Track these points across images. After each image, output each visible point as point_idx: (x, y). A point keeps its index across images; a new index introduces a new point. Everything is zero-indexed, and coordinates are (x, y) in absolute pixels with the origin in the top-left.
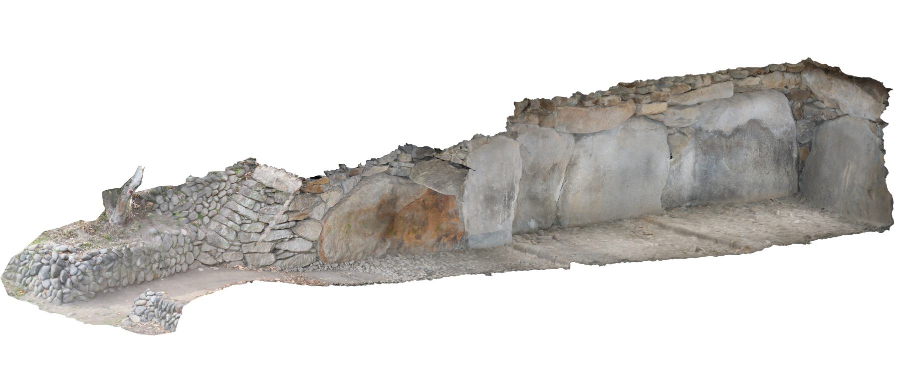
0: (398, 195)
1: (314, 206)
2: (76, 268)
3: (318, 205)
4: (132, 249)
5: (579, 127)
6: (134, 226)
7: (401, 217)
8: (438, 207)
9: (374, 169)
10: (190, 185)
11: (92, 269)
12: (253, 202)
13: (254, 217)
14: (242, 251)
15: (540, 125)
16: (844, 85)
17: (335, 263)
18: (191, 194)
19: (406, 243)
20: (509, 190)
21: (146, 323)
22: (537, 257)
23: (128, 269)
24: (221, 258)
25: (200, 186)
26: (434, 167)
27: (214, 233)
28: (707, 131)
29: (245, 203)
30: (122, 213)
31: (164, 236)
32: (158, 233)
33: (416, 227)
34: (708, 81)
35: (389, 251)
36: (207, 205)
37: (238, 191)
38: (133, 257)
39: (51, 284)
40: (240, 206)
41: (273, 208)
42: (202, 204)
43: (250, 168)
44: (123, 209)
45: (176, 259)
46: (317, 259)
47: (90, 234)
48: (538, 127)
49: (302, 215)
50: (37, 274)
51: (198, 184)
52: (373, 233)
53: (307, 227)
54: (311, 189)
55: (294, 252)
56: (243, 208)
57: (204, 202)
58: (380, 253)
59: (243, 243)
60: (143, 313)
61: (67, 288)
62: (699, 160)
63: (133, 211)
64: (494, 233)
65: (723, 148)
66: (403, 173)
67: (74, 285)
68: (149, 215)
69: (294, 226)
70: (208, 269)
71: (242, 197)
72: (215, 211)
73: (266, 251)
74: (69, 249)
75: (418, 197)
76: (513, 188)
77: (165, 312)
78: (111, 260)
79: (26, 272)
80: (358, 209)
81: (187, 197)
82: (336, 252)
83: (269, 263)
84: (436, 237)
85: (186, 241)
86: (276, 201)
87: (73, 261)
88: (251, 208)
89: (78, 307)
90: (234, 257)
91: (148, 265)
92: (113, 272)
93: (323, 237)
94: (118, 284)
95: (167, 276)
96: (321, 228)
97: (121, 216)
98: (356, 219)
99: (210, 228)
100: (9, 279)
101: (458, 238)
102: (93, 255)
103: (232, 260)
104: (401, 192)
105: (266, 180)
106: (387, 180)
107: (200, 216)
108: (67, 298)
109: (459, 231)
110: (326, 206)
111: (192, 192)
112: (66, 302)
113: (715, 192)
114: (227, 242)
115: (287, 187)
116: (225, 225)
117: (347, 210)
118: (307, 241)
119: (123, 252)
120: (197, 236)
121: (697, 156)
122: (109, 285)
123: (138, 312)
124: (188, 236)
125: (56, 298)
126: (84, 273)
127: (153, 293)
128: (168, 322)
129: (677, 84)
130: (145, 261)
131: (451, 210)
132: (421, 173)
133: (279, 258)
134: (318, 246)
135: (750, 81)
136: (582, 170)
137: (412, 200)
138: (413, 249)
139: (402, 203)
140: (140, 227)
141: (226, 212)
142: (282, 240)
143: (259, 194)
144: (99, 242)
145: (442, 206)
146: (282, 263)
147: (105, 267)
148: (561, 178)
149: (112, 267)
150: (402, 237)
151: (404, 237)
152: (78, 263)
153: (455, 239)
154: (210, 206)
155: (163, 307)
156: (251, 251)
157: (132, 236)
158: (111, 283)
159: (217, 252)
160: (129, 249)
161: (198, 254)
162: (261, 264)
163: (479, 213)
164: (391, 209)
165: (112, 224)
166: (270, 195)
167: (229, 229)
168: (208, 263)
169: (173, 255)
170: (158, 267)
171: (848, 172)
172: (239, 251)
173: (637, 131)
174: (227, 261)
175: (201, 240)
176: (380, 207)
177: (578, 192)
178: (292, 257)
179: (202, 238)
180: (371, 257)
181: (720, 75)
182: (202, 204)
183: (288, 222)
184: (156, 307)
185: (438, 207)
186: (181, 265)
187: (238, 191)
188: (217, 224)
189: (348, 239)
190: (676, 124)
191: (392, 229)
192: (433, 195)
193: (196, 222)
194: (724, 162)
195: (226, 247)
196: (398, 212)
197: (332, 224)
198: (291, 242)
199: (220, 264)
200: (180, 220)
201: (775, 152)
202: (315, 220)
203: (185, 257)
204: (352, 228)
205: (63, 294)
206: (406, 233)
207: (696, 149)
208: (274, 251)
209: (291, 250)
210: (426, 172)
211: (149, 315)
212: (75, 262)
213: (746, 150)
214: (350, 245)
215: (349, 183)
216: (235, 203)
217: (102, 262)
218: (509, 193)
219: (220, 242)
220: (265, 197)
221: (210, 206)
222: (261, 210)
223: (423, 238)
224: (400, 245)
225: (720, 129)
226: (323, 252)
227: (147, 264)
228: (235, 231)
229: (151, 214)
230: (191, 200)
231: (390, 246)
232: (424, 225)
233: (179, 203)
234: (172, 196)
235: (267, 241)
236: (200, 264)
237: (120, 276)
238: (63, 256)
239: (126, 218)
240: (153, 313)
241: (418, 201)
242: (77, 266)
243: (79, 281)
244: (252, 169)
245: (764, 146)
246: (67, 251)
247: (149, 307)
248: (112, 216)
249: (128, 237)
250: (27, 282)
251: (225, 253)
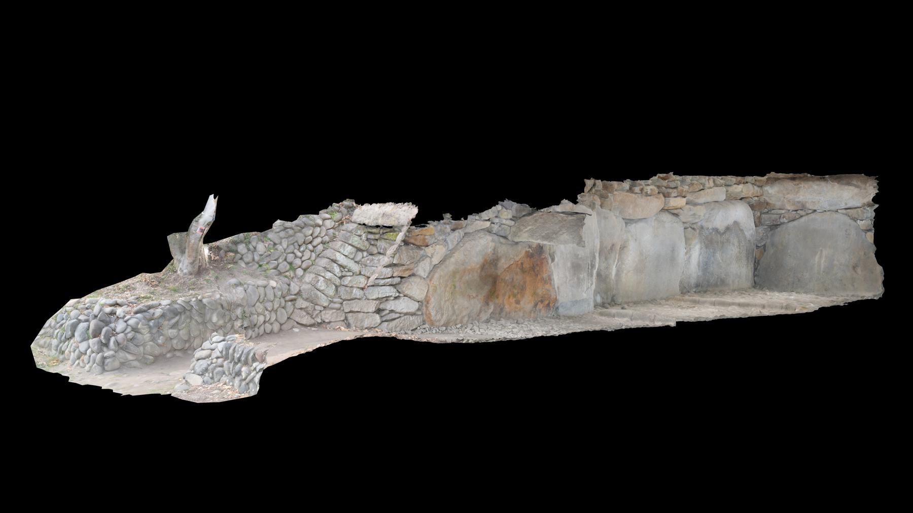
0: (499, 255)
1: (419, 261)
2: (125, 324)
3: (423, 260)
4: (205, 301)
5: (630, 212)
6: (211, 276)
7: (502, 280)
8: (534, 271)
10: (278, 230)
11: (148, 325)
12: (354, 250)
13: (355, 268)
14: (343, 310)
16: (817, 185)
17: (442, 326)
18: (279, 241)
19: (507, 308)
20: (592, 259)
21: (211, 386)
22: (629, 320)
23: (201, 327)
24: (320, 317)
25: (291, 232)
26: (540, 220)
27: (310, 286)
29: (344, 250)
30: (193, 259)
31: (248, 287)
32: (240, 284)
33: (516, 291)
35: (493, 314)
36: (299, 254)
37: (335, 237)
38: (207, 311)
39: (89, 347)
40: (339, 254)
41: (376, 258)
42: (293, 253)
43: (348, 211)
44: (194, 254)
45: (265, 316)
46: (424, 323)
47: (153, 286)
49: (407, 270)
50: (73, 335)
51: (287, 228)
52: (477, 296)
53: (413, 284)
54: (416, 240)
55: (400, 313)
56: (343, 256)
57: (296, 251)
58: (484, 317)
59: (344, 300)
60: (206, 370)
61: (111, 350)
63: (210, 263)
65: (718, 242)
66: (503, 232)
67: (121, 346)
68: (229, 267)
69: (399, 284)
70: (305, 329)
71: (340, 243)
72: (310, 262)
73: (370, 311)
74: (119, 301)
75: (517, 259)
76: (594, 257)
77: (239, 365)
78: (176, 313)
79: (62, 336)
81: (275, 244)
82: (442, 315)
83: (374, 325)
84: (533, 302)
85: (276, 294)
86: (379, 250)
87: (122, 316)
88: (352, 257)
89: (125, 375)
90: (335, 317)
91: (228, 322)
92: (179, 330)
93: (429, 297)
94: (187, 345)
95: (254, 336)
96: (427, 287)
97: (192, 263)
98: (461, 278)
99: (305, 281)
100: (43, 347)
101: (551, 305)
102: (150, 307)
103: (332, 320)
105: (370, 218)
106: (489, 238)
107: (292, 266)
108: (109, 364)
109: (552, 297)
110: (431, 262)
111: (281, 238)
112: (109, 369)
113: (712, 281)
114: (325, 297)
115: (398, 219)
116: (323, 277)
117: (452, 268)
118: (413, 301)
119: (192, 303)
120: (289, 290)
121: (701, 249)
122: (174, 346)
123: (198, 370)
124: (279, 289)
125: (95, 364)
126: (135, 330)
127: (222, 338)
128: (245, 379)
129: (693, 182)
130: (224, 316)
131: (545, 276)
132: (524, 229)
133: (384, 319)
134: (424, 308)
137: (512, 263)
138: (513, 314)
139: (503, 264)
140: (217, 278)
141: (323, 262)
142: (387, 299)
143: (361, 239)
144: (161, 294)
145: (538, 271)
146: (388, 325)
147: (166, 323)
148: (616, 258)
149: (177, 323)
150: (503, 301)
151: (505, 302)
152: (128, 317)
153: (548, 305)
154: (303, 256)
155: (237, 355)
156: (353, 310)
157: (206, 287)
158: (177, 343)
159: (315, 309)
160: (201, 301)
161: (291, 311)
162: (366, 326)
163: (568, 280)
164: (493, 270)
165: (181, 275)
166: (372, 243)
167: (328, 281)
168: (304, 322)
169: (261, 311)
170: (242, 326)
171: (821, 257)
173: (665, 222)
174: (327, 321)
175: (295, 295)
176: (483, 267)
177: (629, 271)
178: (398, 318)
179: (296, 292)
180: (476, 322)
182: (293, 253)
183: (392, 277)
184: (226, 358)
185: (534, 271)
186: (271, 324)
187: (335, 237)
188: (313, 276)
189: (454, 301)
190: (690, 219)
192: (530, 258)
193: (287, 274)
194: (718, 255)
195: (325, 304)
196: (499, 274)
197: (438, 283)
198: (397, 301)
199: (319, 324)
200: (268, 272)
202: (420, 277)
203: (276, 314)
204: (457, 289)
205: (104, 358)
206: (507, 297)
208: (379, 311)
209: (397, 311)
210: (530, 227)
211: (215, 372)
212: (125, 316)
214: (456, 307)
216: (333, 251)
217: (163, 316)
218: (592, 261)
219: (317, 296)
220: (366, 243)
221: (303, 256)
222: (363, 260)
224: (502, 310)
226: (430, 314)
227: (226, 321)
228: (334, 284)
229: (232, 265)
230: (280, 247)
231: (493, 310)
233: (265, 252)
234: (257, 243)
235: (371, 298)
236: (296, 323)
237: (190, 334)
238: (108, 310)
239: (200, 267)
240: (220, 369)
242: (126, 322)
243: (128, 341)
244: (350, 212)
245: (742, 245)
246: (116, 304)
247: (215, 360)
248: (181, 264)
249: (201, 288)
250: (63, 349)
251: (324, 312)
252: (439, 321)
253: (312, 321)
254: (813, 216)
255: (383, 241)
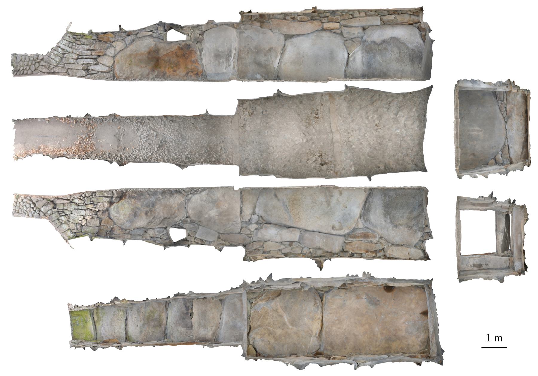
0: (159, 48)
7: (162, 59)
9: (142, 33)
13: (70, 50)
15: (261, 27)
28: (368, 41)
34: (363, 14)
48: (260, 28)
59: (65, 64)
62: (364, 56)
64: (221, 73)
73: (79, 69)
75: (172, 50)
80: (135, 53)
82: (124, 74)
104: (161, 47)
113: (376, 73)
117: (129, 53)
121: (362, 53)
135: (389, 17)
136: (289, 53)
137: (169, 52)
153: (197, 74)
156: (70, 68)
163: (212, 62)
171: (478, 131)
172: (63, 67)
176: (149, 53)
177: (286, 63)
178: (97, 73)
179: (40, 59)
181: (370, 12)
191: (158, 65)
194: (378, 58)
198: (95, 66)
201: (410, 56)
202: (109, 56)
204: (133, 63)
206: (167, 68)
207: (362, 50)
213: (391, 52)
215: (129, 39)
219: (50, 61)
223: (178, 72)
225: (374, 40)
232: (177, 65)
241: (172, 52)
252: (122, 76)
253: (49, 71)
254: (503, 122)
255: (83, 39)
